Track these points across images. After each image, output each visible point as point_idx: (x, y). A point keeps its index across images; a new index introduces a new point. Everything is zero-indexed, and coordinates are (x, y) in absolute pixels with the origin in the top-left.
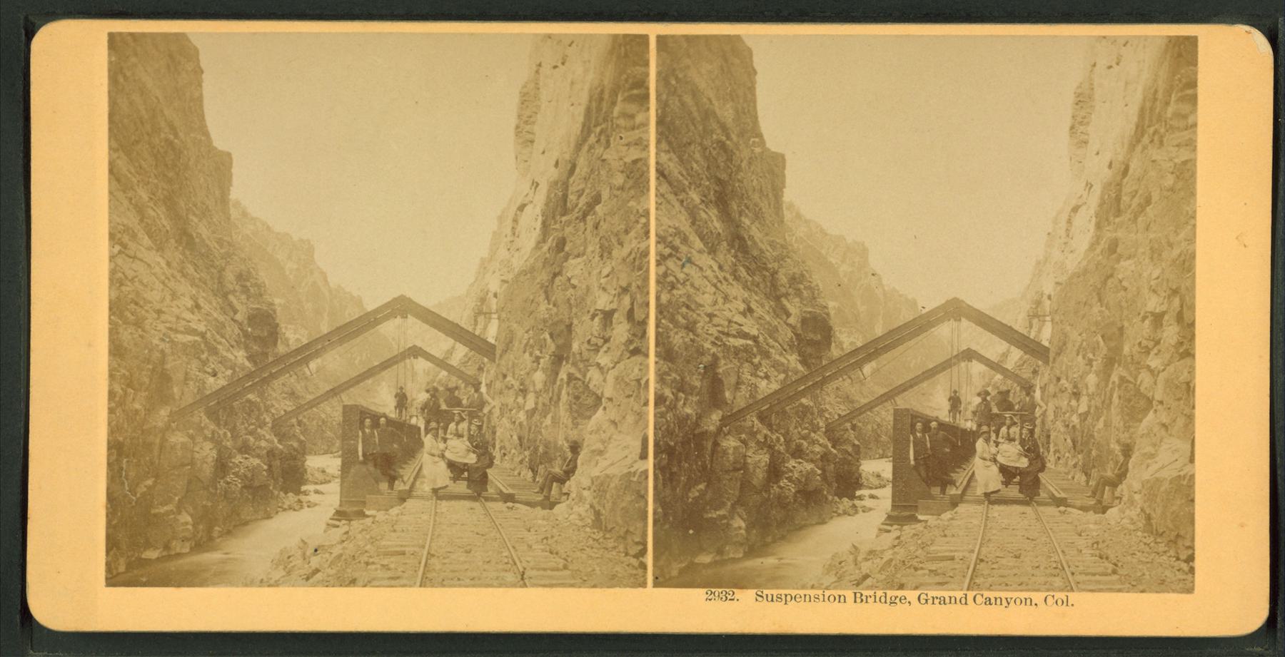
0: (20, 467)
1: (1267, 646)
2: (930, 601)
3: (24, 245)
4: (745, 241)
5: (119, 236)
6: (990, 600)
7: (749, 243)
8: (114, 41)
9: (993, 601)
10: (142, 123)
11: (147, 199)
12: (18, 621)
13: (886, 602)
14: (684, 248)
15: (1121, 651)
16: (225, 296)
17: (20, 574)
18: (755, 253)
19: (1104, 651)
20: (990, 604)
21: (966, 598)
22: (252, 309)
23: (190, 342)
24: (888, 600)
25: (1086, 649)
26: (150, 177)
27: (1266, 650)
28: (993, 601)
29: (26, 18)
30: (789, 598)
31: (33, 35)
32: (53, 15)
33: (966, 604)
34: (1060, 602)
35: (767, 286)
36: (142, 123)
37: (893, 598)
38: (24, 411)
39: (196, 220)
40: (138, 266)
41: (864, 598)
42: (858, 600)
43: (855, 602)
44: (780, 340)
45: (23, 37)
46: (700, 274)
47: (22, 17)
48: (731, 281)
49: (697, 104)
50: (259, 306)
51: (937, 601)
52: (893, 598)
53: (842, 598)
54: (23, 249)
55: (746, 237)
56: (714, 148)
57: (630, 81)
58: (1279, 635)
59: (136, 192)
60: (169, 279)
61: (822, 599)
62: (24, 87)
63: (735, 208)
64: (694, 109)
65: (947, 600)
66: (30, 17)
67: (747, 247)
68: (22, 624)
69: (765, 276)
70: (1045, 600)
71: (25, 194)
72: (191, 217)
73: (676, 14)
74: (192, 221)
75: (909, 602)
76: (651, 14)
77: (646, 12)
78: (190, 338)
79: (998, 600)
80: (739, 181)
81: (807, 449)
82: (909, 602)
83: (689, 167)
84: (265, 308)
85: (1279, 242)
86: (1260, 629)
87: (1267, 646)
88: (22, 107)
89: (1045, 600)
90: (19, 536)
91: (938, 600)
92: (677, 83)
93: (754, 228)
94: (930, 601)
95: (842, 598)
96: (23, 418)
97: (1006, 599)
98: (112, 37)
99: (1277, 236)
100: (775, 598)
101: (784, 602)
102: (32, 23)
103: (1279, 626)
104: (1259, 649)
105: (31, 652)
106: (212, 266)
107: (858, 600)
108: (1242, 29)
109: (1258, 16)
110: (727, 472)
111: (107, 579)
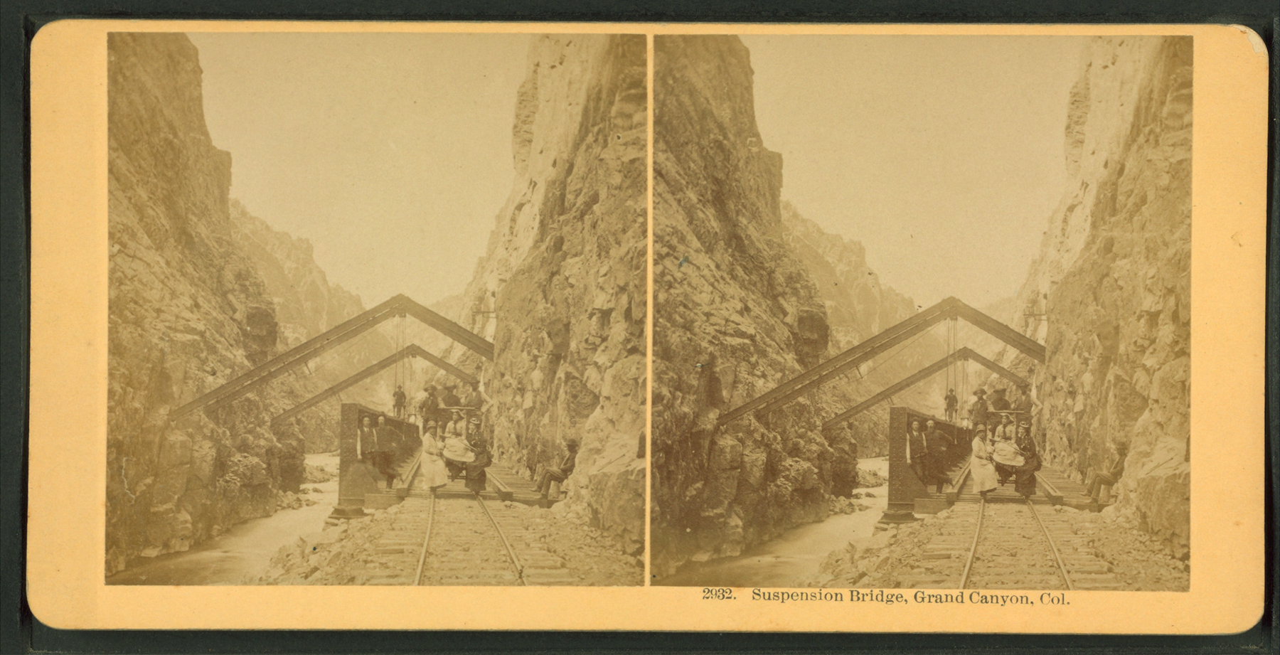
0: (20, 466)
1: (1262, 644)
2: (926, 600)
3: (24, 244)
4: (742, 241)
5: (118, 235)
6: (986, 598)
7: (746, 242)
8: (114, 41)
9: (989, 599)
10: (142, 123)
11: (146, 198)
12: (18, 619)
13: (882, 600)
14: (131, 244)
15: (1117, 649)
16: (775, 298)
17: (20, 572)
18: (752, 252)
19: (1100, 649)
20: (986, 602)
21: (962, 596)
22: (251, 308)
23: (740, 345)
24: (885, 599)
25: (1082, 647)
26: (149, 176)
27: (1261, 648)
28: (989, 599)
29: (26, 18)
30: (786, 596)
31: (33, 35)
32: (53, 15)
33: (962, 602)
34: (1055, 600)
35: (763, 285)
36: (142, 123)
37: (890, 597)
38: (24, 409)
39: (195, 219)
40: (138, 265)
41: (860, 596)
42: (855, 598)
43: (852, 600)
44: (777, 339)
45: (23, 37)
46: (697, 274)
47: (22, 17)
48: (728, 280)
49: (694, 104)
50: (258, 305)
51: (933, 599)
52: (890, 597)
53: (839, 596)
54: (23, 248)
55: (743, 236)
56: (162, 147)
57: (1179, 80)
58: (1274, 633)
59: (136, 191)
60: (168, 279)
61: (818, 597)
62: (24, 87)
63: (733, 207)
64: (691, 109)
65: (944, 598)
66: (30, 17)
67: (744, 246)
68: (22, 621)
69: (762, 275)
70: (1041, 599)
71: (25, 194)
72: (190, 216)
73: (673, 14)
74: (191, 220)
75: (906, 601)
76: (649, 14)
77: (644, 12)
78: (189, 337)
79: (995, 599)
80: (186, 178)
81: (804, 447)
82: (906, 601)
83: (686, 166)
84: (264, 307)
85: (1274, 242)
86: (1255, 627)
87: (1262, 644)
88: (22, 106)
89: (1041, 599)
90: (19, 534)
91: (935, 598)
92: (674, 82)
93: (750, 227)
94: (926, 600)
95: (839, 596)
96: (23, 417)
97: (1003, 597)
98: (111, 36)
99: (1272, 235)
100: (772, 596)
101: (781, 600)
102: (32, 23)
103: (1274, 624)
104: (1255, 647)
105: (31, 650)
106: (211, 265)
107: (855, 598)
108: (1237, 29)
109: (1253, 16)
110: (724, 470)
111: (106, 577)
